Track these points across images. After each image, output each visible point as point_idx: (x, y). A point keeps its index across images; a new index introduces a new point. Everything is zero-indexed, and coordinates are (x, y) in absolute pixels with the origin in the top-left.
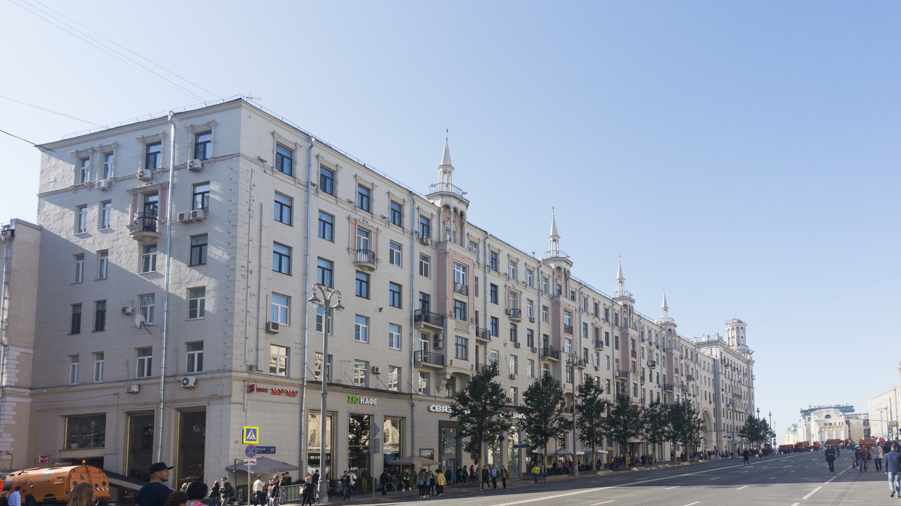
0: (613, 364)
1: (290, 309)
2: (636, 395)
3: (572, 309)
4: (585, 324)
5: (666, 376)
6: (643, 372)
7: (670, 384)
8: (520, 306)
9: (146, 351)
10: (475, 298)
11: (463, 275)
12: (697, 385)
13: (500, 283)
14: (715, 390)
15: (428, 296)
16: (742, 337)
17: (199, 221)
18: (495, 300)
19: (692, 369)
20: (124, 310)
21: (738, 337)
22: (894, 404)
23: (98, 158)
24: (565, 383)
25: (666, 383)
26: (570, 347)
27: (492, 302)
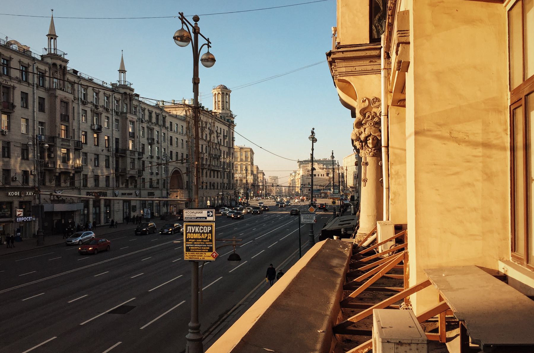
3: (135, 120)
8: (13, 100)
21: (223, 102)
22: (404, 32)
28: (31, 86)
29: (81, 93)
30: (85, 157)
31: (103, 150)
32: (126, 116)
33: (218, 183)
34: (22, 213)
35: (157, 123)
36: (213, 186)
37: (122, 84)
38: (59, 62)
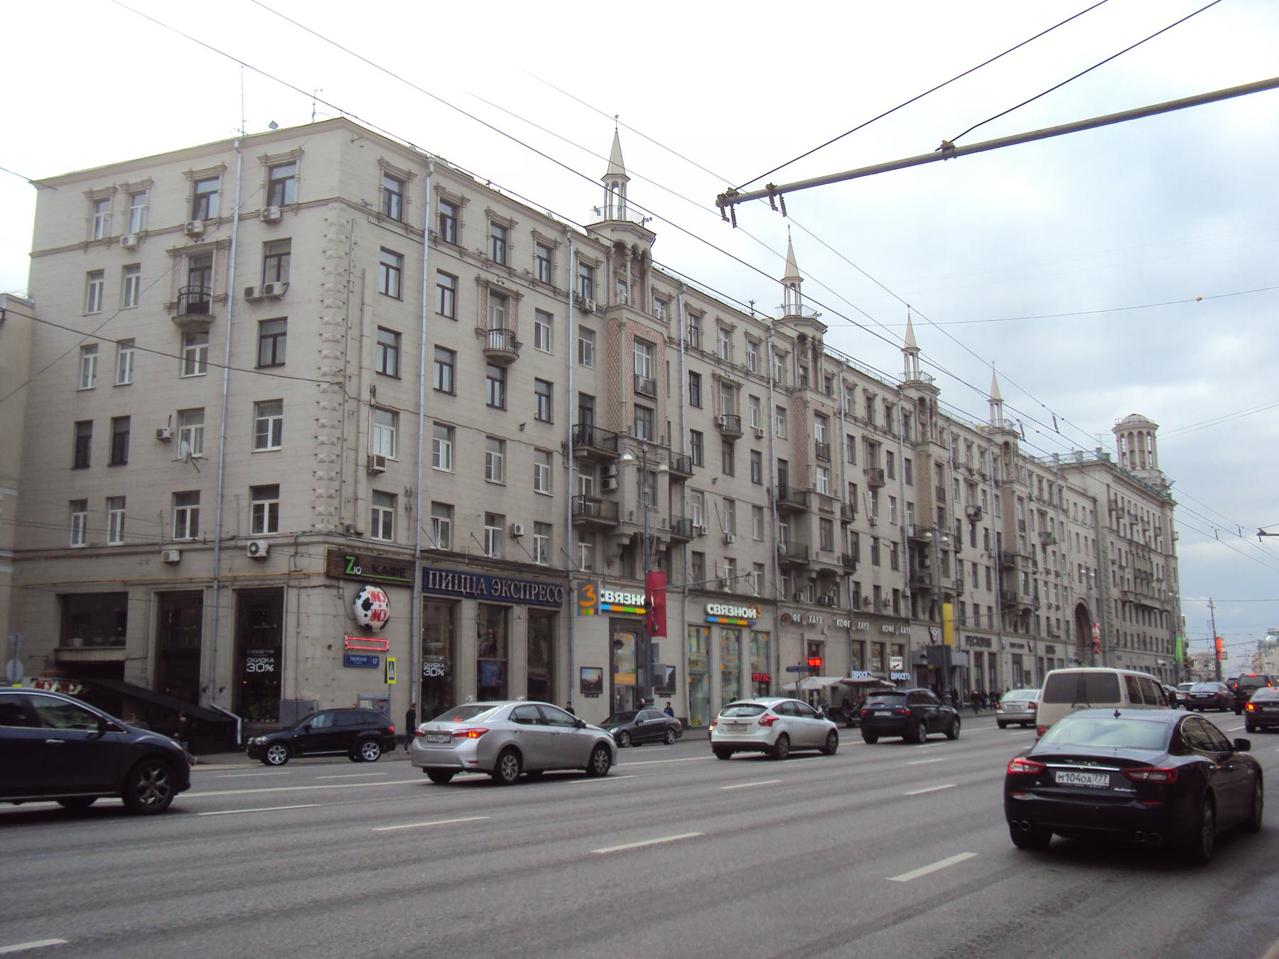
1: (552, 470)
2: (1026, 592)
4: (851, 438)
6: (959, 529)
7: (1011, 551)
9: (184, 498)
10: (667, 399)
11: (647, 359)
12: (1063, 552)
13: (705, 370)
14: (1099, 561)
15: (592, 398)
16: (1150, 452)
17: (277, 299)
18: (696, 403)
19: (1052, 519)
20: (160, 433)
23: (121, 198)
24: (819, 551)
25: (1003, 547)
26: (825, 481)
27: (691, 404)
28: (675, 347)
29: (774, 365)
31: (714, 481)
34: (901, 663)
35: (888, 431)
36: (1144, 642)
37: (793, 313)
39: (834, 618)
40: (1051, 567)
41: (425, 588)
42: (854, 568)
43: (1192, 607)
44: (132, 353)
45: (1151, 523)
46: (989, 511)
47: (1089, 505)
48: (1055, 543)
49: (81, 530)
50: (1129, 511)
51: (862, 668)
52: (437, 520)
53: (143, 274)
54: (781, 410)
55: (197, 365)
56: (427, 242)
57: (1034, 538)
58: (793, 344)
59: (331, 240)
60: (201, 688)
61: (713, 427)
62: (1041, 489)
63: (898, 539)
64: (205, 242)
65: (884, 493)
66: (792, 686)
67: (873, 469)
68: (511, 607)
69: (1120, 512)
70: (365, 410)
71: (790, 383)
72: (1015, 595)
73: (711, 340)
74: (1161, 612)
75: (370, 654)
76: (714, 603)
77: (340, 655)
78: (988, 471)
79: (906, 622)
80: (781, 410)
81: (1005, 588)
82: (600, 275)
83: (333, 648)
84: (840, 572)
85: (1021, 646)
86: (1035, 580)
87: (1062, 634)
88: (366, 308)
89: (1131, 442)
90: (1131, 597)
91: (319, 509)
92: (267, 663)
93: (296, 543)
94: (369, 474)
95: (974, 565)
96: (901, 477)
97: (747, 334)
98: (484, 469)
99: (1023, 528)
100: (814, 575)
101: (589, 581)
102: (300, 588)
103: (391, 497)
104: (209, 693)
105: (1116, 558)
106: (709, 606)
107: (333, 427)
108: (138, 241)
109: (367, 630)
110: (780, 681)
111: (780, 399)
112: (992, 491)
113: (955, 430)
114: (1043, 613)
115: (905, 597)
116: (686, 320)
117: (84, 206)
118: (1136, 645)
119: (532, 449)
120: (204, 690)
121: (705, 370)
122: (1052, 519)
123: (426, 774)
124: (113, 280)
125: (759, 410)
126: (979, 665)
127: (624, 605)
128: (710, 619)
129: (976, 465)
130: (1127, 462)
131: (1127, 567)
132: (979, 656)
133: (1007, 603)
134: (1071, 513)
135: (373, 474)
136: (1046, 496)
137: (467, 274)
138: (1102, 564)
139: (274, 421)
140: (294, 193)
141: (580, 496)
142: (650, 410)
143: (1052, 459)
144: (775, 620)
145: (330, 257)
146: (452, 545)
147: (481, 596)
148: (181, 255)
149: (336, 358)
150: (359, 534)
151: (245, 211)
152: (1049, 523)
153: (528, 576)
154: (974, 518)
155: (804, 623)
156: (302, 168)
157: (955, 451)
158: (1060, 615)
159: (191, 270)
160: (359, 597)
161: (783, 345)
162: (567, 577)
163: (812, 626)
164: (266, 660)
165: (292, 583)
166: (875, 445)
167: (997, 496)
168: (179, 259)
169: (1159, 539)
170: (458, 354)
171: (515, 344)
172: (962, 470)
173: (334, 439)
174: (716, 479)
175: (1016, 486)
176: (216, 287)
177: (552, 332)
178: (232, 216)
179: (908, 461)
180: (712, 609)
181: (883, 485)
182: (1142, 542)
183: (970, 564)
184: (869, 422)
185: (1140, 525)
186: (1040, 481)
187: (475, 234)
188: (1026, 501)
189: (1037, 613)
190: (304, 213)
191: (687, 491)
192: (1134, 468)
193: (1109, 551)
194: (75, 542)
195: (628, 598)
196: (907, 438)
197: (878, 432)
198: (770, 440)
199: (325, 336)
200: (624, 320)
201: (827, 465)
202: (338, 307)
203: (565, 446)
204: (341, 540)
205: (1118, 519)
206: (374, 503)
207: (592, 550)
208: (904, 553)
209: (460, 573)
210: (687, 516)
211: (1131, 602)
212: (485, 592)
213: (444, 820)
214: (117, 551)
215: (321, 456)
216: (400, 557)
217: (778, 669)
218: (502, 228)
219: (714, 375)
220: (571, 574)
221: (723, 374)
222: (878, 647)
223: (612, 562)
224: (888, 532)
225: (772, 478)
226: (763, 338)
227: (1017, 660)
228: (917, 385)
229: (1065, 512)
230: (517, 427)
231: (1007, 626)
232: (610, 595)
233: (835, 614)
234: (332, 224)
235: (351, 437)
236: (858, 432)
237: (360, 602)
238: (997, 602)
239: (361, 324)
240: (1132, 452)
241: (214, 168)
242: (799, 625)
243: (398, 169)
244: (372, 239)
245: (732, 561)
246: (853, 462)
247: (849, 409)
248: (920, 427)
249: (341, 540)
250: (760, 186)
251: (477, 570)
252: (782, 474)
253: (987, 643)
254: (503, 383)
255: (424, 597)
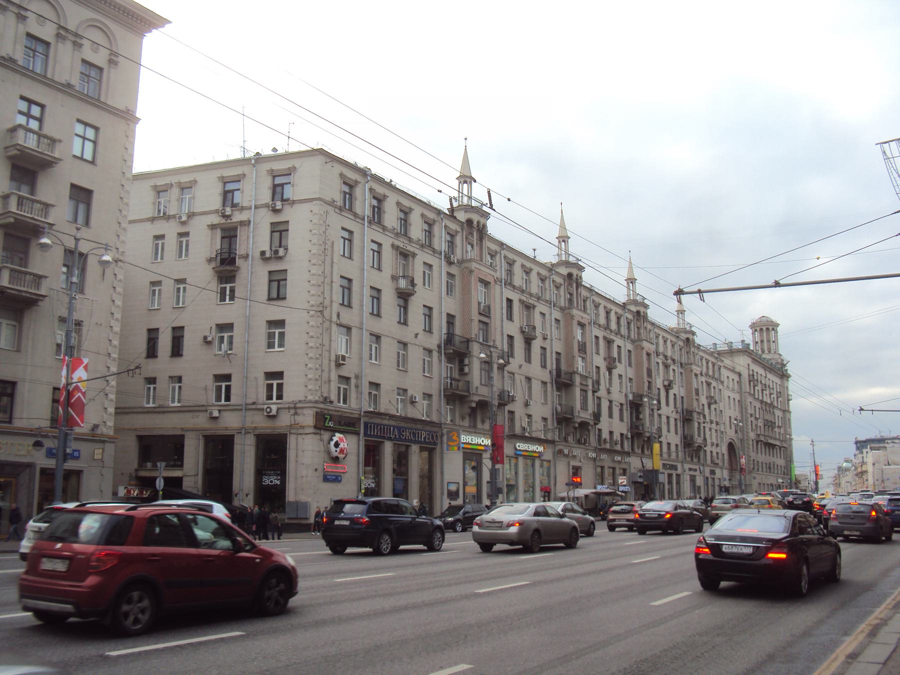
0: (626, 384)
1: (432, 361)
2: (699, 435)
4: (597, 337)
5: (562, 356)
6: (659, 395)
7: (690, 409)
11: (485, 292)
13: (515, 297)
14: (742, 414)
16: (774, 342)
17: (281, 258)
18: (510, 318)
19: (714, 387)
20: (205, 338)
24: (580, 410)
29: (554, 293)
30: (404, 353)
31: (520, 366)
32: (691, 368)
33: (770, 464)
34: (625, 481)
35: (618, 333)
36: (770, 468)
38: (475, 218)
39: (587, 452)
40: (713, 418)
41: (365, 435)
42: (599, 421)
43: (800, 443)
44: (185, 288)
45: (775, 389)
46: (677, 383)
47: (736, 378)
48: (716, 402)
49: (151, 397)
50: (761, 381)
51: (602, 484)
52: (371, 393)
53: (191, 238)
54: (557, 321)
55: (228, 297)
56: (366, 224)
57: (704, 400)
58: (564, 280)
59: (315, 224)
60: (234, 495)
61: (520, 333)
62: (708, 368)
63: (623, 402)
64: (232, 221)
65: (615, 372)
66: (564, 494)
67: (609, 357)
68: (410, 446)
69: (756, 382)
70: (334, 328)
71: (562, 304)
72: (692, 437)
73: (518, 279)
74: (780, 448)
75: (337, 474)
76: (520, 443)
77: (322, 475)
78: (676, 357)
79: (628, 454)
80: (557, 321)
81: (686, 432)
82: (458, 240)
83: (318, 470)
84: (592, 423)
85: (695, 470)
86: (704, 427)
87: (719, 462)
88: (335, 266)
89: (761, 335)
90: (762, 438)
91: (310, 387)
92: (276, 479)
93: (295, 408)
94: (336, 365)
95: (668, 417)
96: (626, 362)
97: (538, 274)
98: (396, 361)
99: (697, 394)
100: (577, 425)
101: (453, 430)
102: (298, 434)
103: (347, 379)
104: (240, 496)
105: (753, 412)
106: (518, 444)
107: (318, 337)
108: (188, 218)
109: (336, 460)
110: (557, 491)
111: (557, 314)
112: (678, 370)
113: (657, 330)
114: (708, 449)
115: (627, 438)
116: (445, 237)
117: (150, 196)
118: (765, 470)
119: (421, 349)
120: (236, 495)
121: (515, 297)
122: (714, 387)
123: (328, 548)
124: (171, 242)
125: (545, 321)
126: (670, 483)
127: (471, 444)
128: (518, 453)
129: (669, 354)
130: (759, 348)
131: (760, 418)
132: (670, 476)
133: (687, 442)
134: (725, 384)
135: (338, 365)
136: (711, 373)
137: (387, 242)
138: (744, 417)
139: (279, 333)
140: (288, 193)
141: (447, 378)
142: (486, 324)
143: (712, 347)
144: (554, 453)
145: (314, 234)
146: (380, 408)
147: (395, 439)
148: (217, 228)
149: (319, 296)
150: (331, 402)
151: (259, 203)
152: (712, 390)
153: (419, 427)
154: (668, 388)
155: (570, 455)
156: (295, 178)
157: (657, 344)
158: (718, 450)
159: (223, 238)
160: (332, 440)
161: (559, 280)
162: (441, 427)
163: (574, 457)
164: (275, 477)
165: (292, 431)
166: (408, 255)
167: (681, 373)
168: (215, 231)
169: (780, 399)
170: (383, 292)
171: (413, 284)
172: (661, 357)
173: (318, 345)
174: (418, 334)
175: (693, 367)
176: (240, 250)
177: (432, 277)
178: (251, 206)
179: (629, 351)
180: (519, 446)
181: (615, 367)
182: (769, 402)
183: (665, 417)
184: (607, 327)
185: (768, 391)
186: (707, 363)
187: (391, 218)
188: (699, 376)
189: (705, 448)
190: (296, 206)
191: (506, 373)
192: (763, 352)
193: (749, 408)
194: (148, 402)
195: (474, 440)
196: (629, 337)
197: (612, 334)
198: (552, 340)
199: (313, 282)
200: (473, 268)
201: (584, 356)
202: (320, 265)
203: (439, 346)
204: (322, 406)
205: (754, 387)
206: (339, 383)
207: (453, 411)
208: (627, 410)
209: (384, 425)
210: (506, 389)
211: (762, 441)
212: (397, 437)
213: (372, 575)
214: (176, 409)
215: (310, 355)
216: (353, 416)
217: (556, 484)
218: (406, 213)
219: (520, 300)
220: (443, 425)
221: (525, 299)
222: (611, 470)
223: (465, 418)
224: (618, 397)
225: (441, 328)
226: (498, 250)
227: (693, 479)
228: (635, 302)
229: (722, 382)
230: (413, 336)
231: (687, 457)
232: (465, 438)
233: (588, 449)
234: (315, 214)
235: (326, 343)
236: (600, 333)
237: (332, 443)
238: (681, 442)
239: (332, 274)
240: (762, 341)
241: (238, 175)
242: (567, 456)
243: (350, 179)
244: (338, 222)
245: (529, 416)
246: (598, 353)
247: (556, 300)
248: (636, 329)
249: (322, 406)
250: (696, 289)
251: (392, 423)
252: (558, 361)
253: (675, 468)
254: (406, 308)
255: (365, 440)
